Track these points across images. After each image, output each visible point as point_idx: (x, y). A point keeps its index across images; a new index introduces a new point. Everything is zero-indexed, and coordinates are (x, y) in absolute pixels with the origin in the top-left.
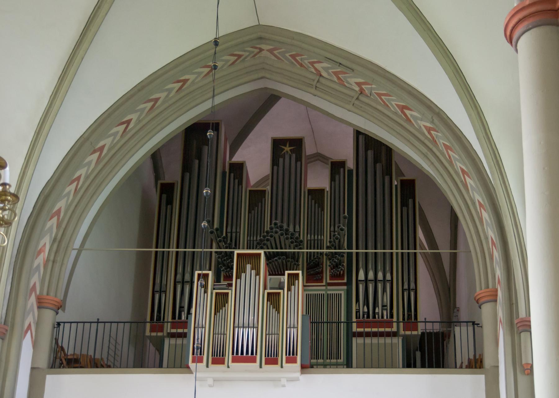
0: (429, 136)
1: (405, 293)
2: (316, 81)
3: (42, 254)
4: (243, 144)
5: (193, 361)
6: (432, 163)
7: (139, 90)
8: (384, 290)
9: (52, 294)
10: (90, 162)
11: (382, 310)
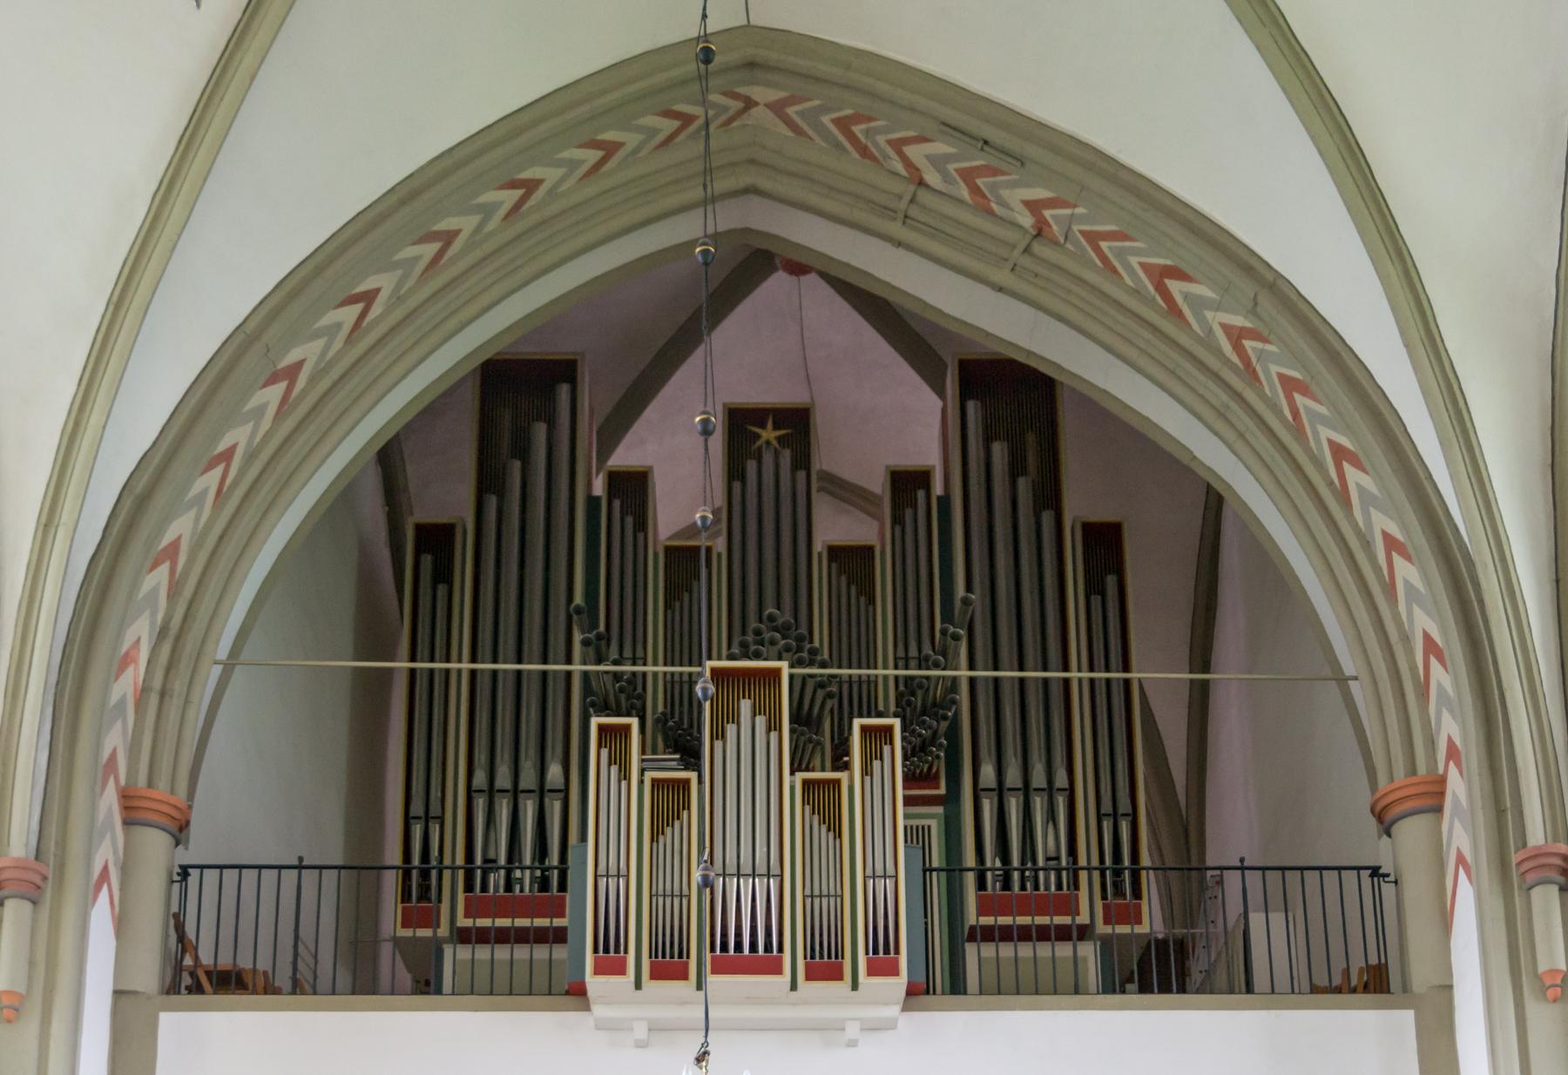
0: (1235, 359)
1: (1105, 824)
2: (908, 197)
3: (130, 671)
4: (636, 426)
5: (598, 970)
7: (403, 202)
8: (1051, 815)
9: (163, 784)
10: (260, 411)
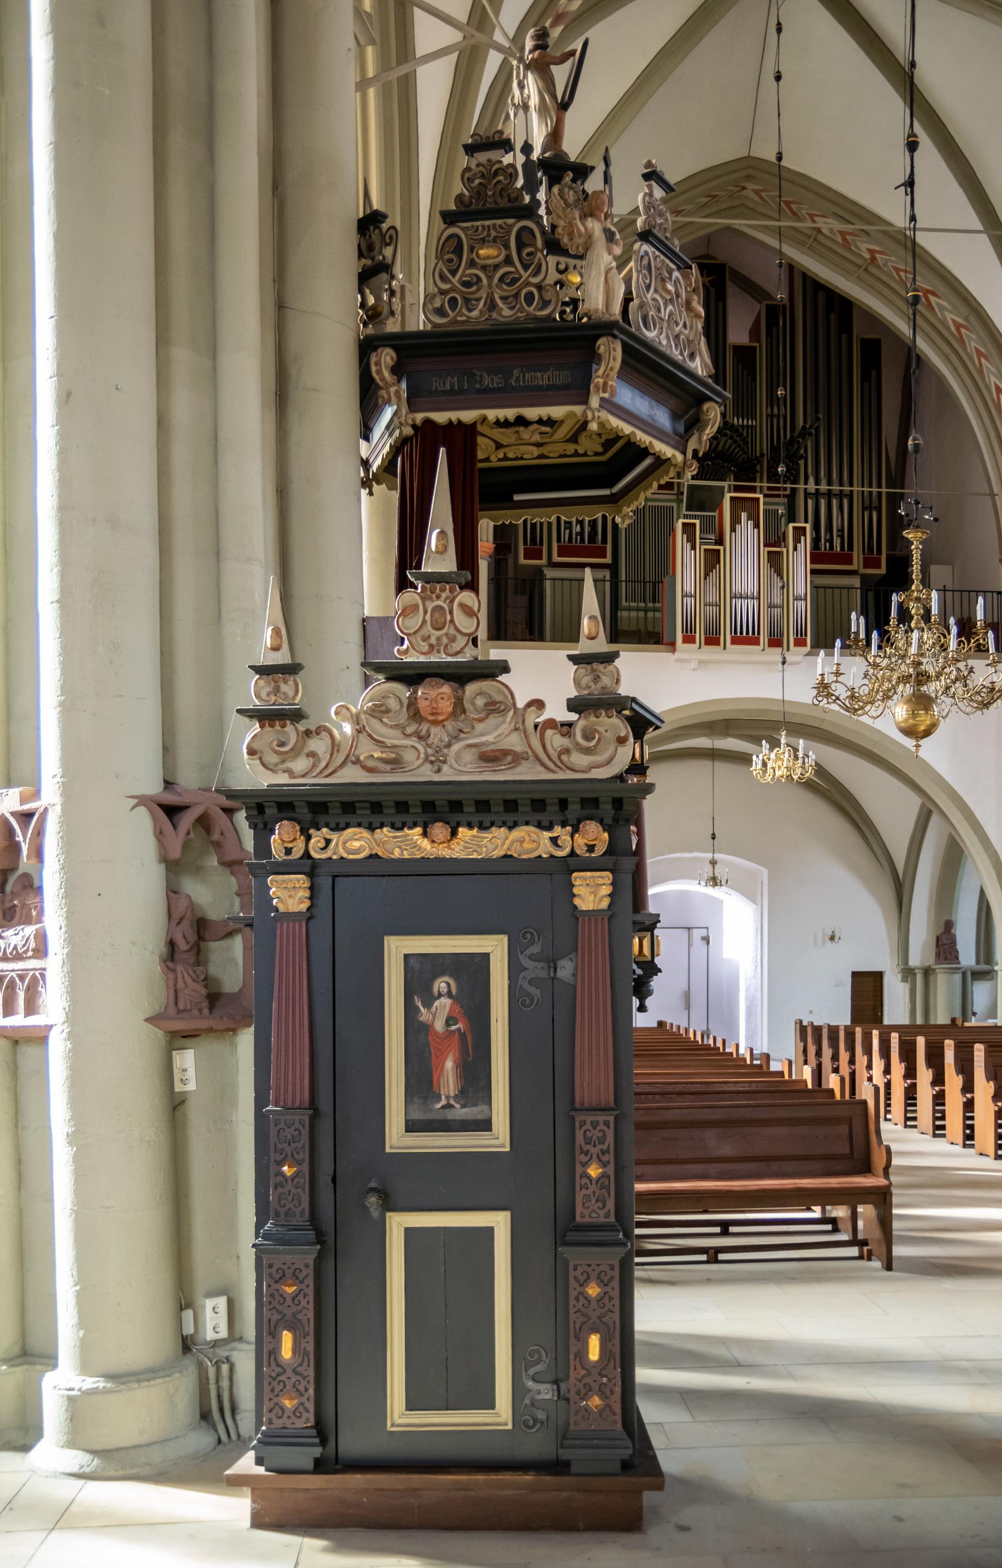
0: (955, 332)
6: (955, 369)
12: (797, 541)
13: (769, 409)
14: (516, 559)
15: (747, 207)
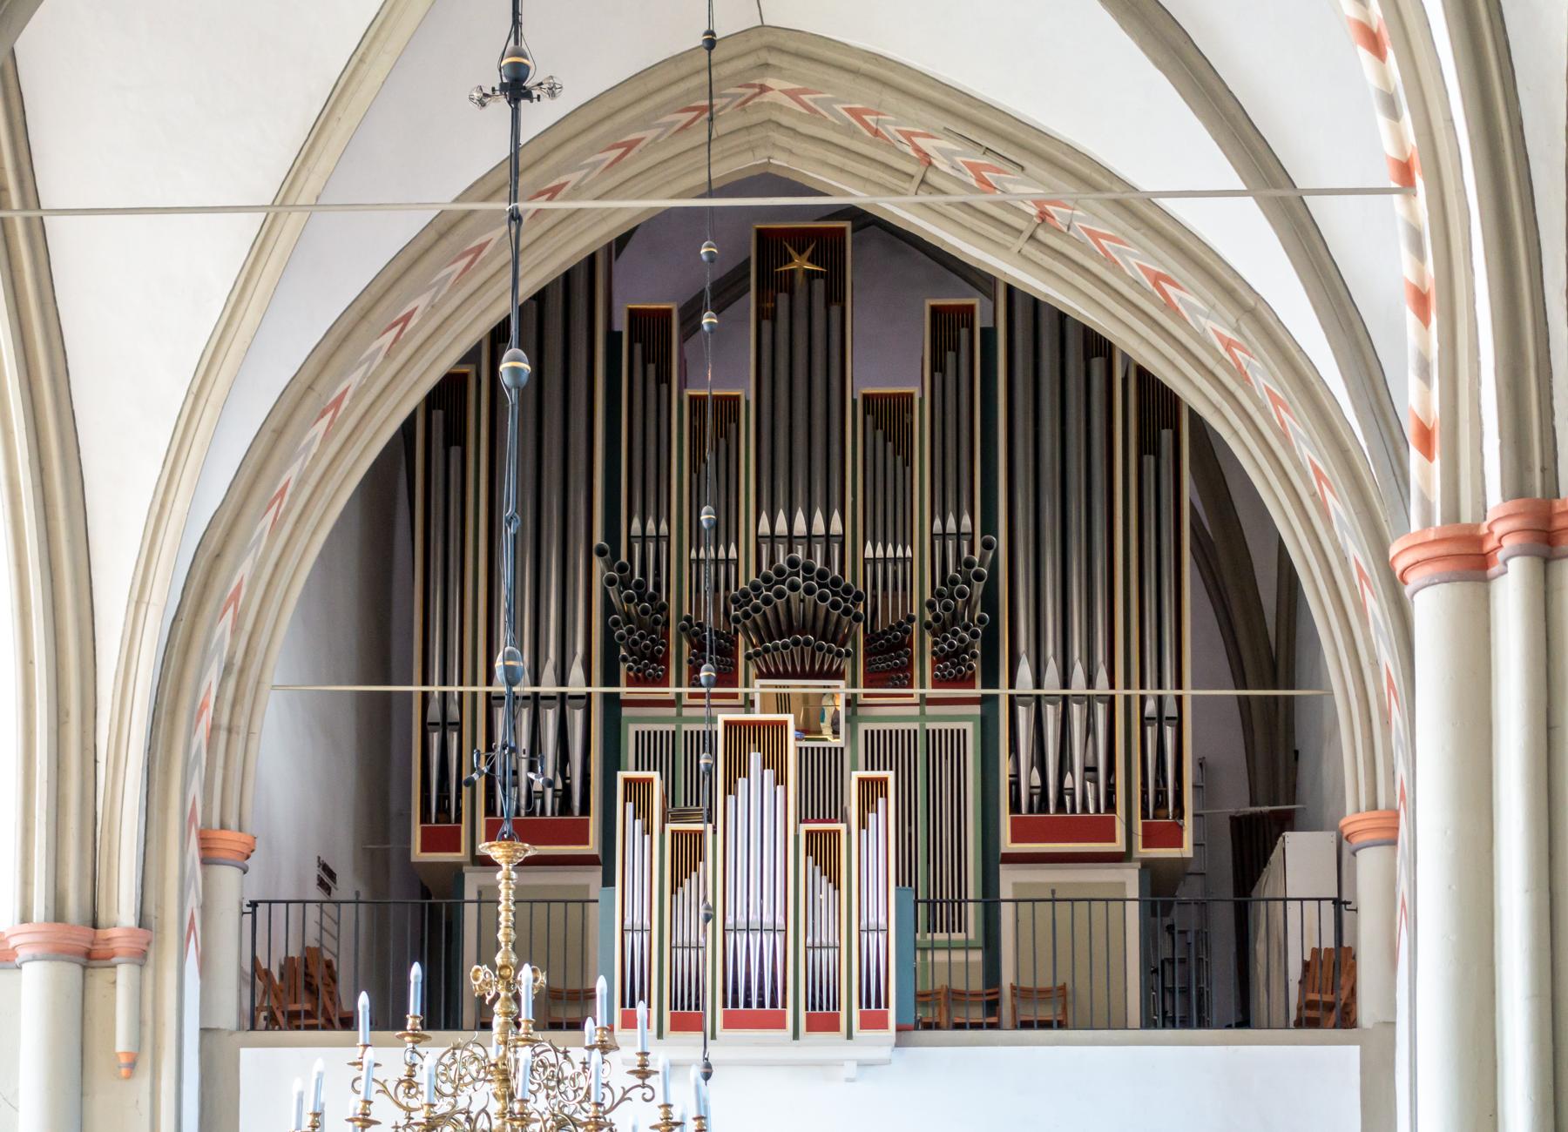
0: (1227, 356)
7: (442, 236)
11: (1084, 780)
12: (867, 805)
13: (938, 522)
14: (407, 852)
15: (779, 125)
